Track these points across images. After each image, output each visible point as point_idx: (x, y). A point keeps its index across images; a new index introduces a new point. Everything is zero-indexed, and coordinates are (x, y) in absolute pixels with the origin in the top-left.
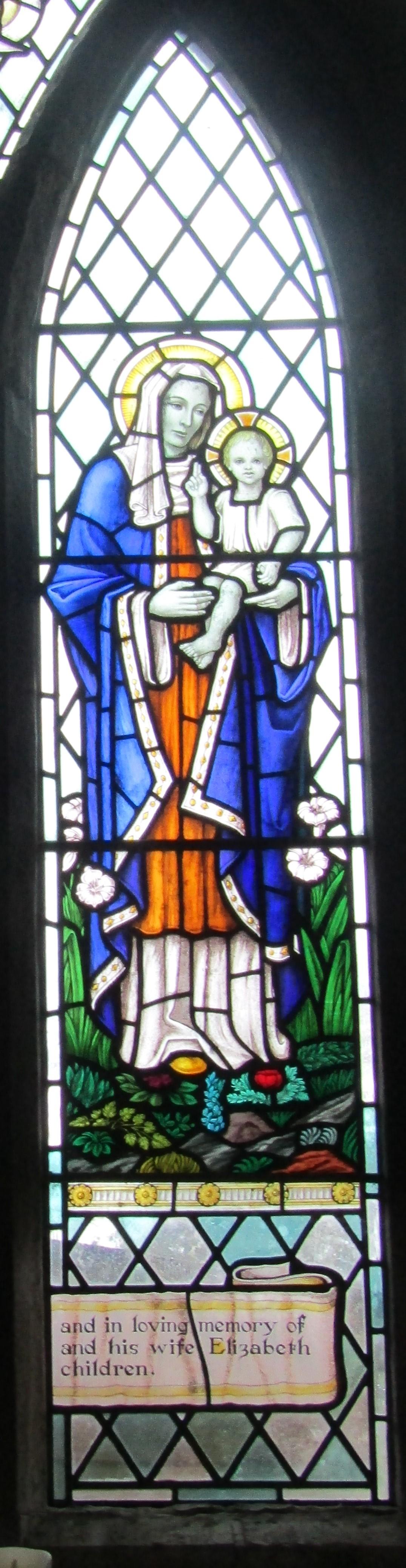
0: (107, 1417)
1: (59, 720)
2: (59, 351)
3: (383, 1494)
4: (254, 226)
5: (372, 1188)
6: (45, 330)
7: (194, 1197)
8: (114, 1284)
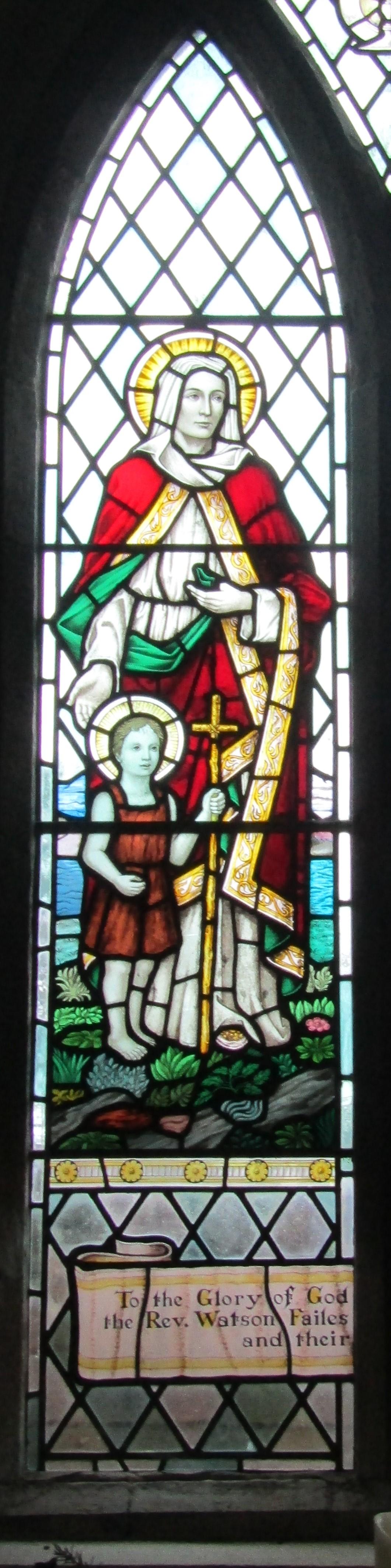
0: (227, 1388)
1: (333, 719)
2: (71, 339)
3: (348, 1461)
4: (265, 221)
5: (347, 1164)
6: (58, 319)
7: (307, 1174)
8: (242, 1258)
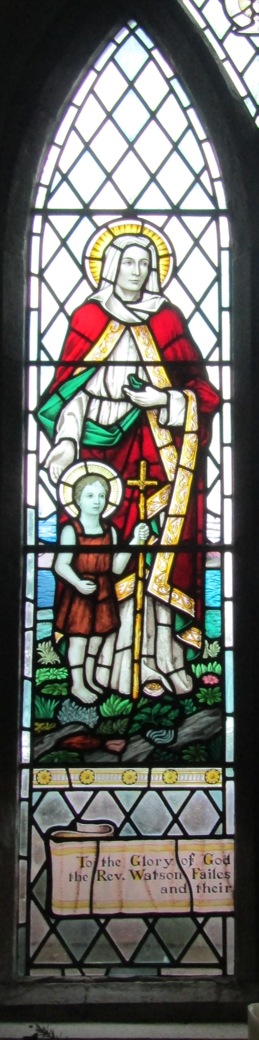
0: (151, 920)
1: (220, 477)
2: (47, 225)
3: (231, 969)
4: (175, 147)
5: (230, 772)
6: (38, 212)
7: (203, 778)
8: (160, 834)
